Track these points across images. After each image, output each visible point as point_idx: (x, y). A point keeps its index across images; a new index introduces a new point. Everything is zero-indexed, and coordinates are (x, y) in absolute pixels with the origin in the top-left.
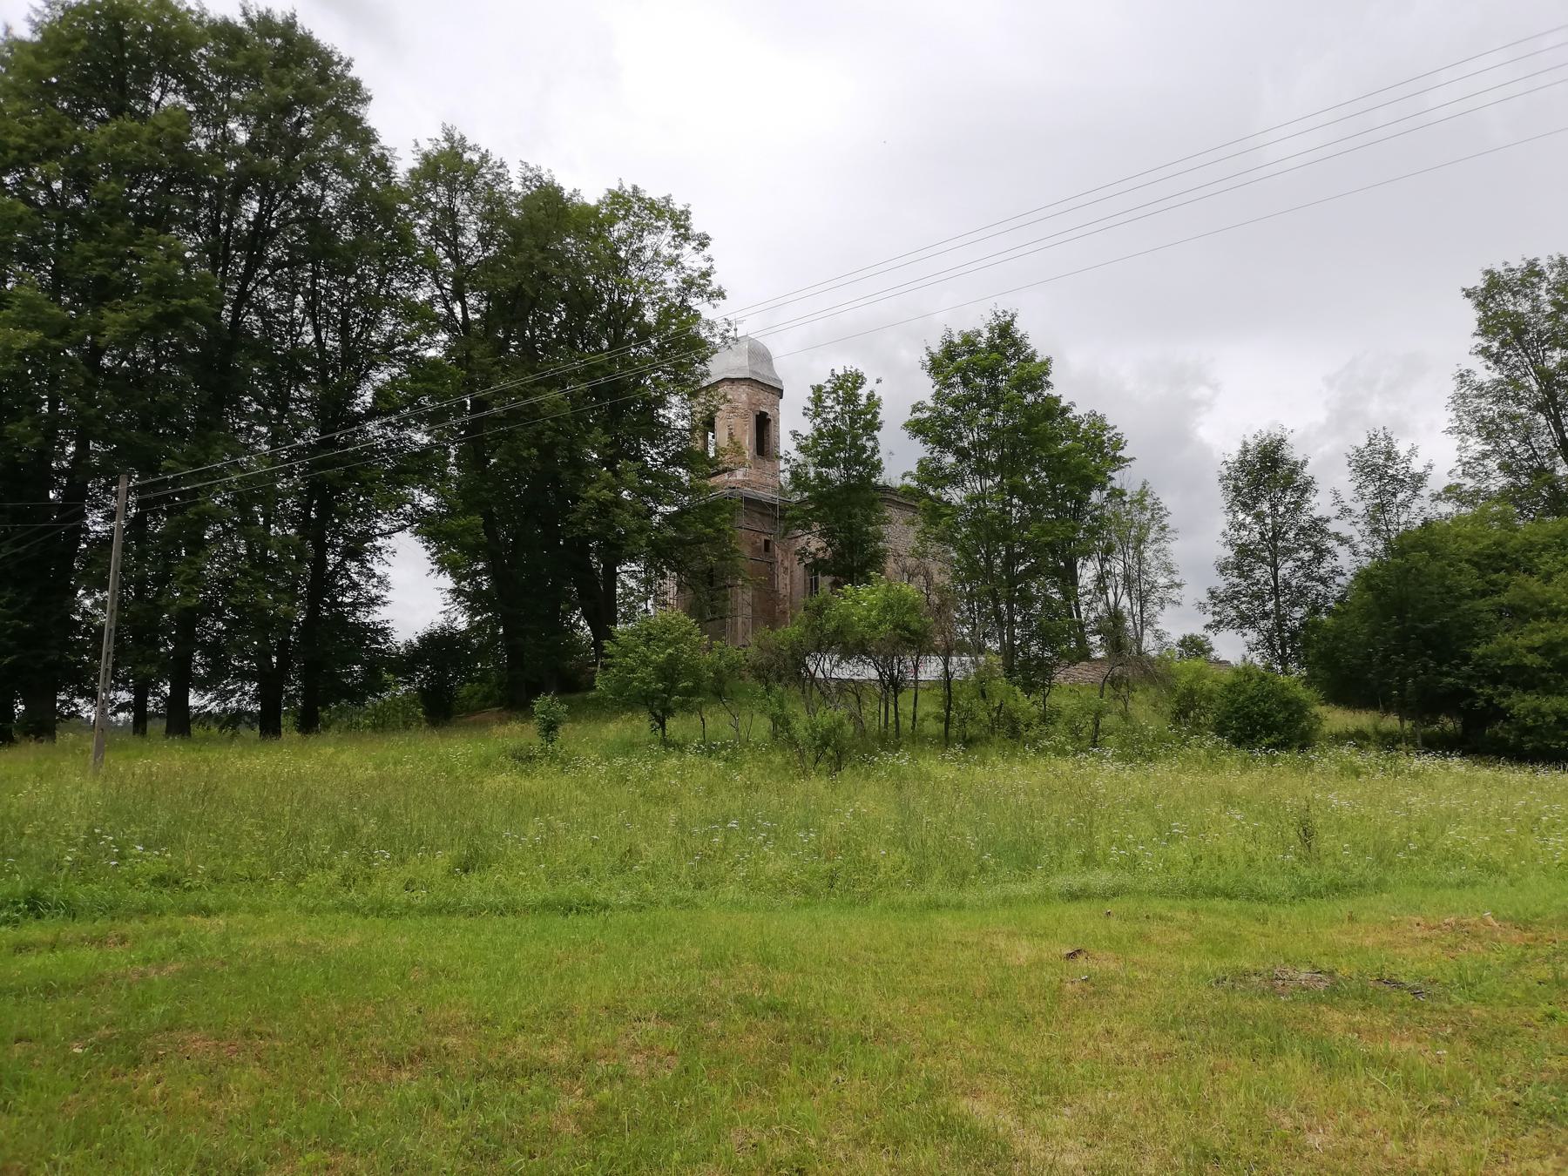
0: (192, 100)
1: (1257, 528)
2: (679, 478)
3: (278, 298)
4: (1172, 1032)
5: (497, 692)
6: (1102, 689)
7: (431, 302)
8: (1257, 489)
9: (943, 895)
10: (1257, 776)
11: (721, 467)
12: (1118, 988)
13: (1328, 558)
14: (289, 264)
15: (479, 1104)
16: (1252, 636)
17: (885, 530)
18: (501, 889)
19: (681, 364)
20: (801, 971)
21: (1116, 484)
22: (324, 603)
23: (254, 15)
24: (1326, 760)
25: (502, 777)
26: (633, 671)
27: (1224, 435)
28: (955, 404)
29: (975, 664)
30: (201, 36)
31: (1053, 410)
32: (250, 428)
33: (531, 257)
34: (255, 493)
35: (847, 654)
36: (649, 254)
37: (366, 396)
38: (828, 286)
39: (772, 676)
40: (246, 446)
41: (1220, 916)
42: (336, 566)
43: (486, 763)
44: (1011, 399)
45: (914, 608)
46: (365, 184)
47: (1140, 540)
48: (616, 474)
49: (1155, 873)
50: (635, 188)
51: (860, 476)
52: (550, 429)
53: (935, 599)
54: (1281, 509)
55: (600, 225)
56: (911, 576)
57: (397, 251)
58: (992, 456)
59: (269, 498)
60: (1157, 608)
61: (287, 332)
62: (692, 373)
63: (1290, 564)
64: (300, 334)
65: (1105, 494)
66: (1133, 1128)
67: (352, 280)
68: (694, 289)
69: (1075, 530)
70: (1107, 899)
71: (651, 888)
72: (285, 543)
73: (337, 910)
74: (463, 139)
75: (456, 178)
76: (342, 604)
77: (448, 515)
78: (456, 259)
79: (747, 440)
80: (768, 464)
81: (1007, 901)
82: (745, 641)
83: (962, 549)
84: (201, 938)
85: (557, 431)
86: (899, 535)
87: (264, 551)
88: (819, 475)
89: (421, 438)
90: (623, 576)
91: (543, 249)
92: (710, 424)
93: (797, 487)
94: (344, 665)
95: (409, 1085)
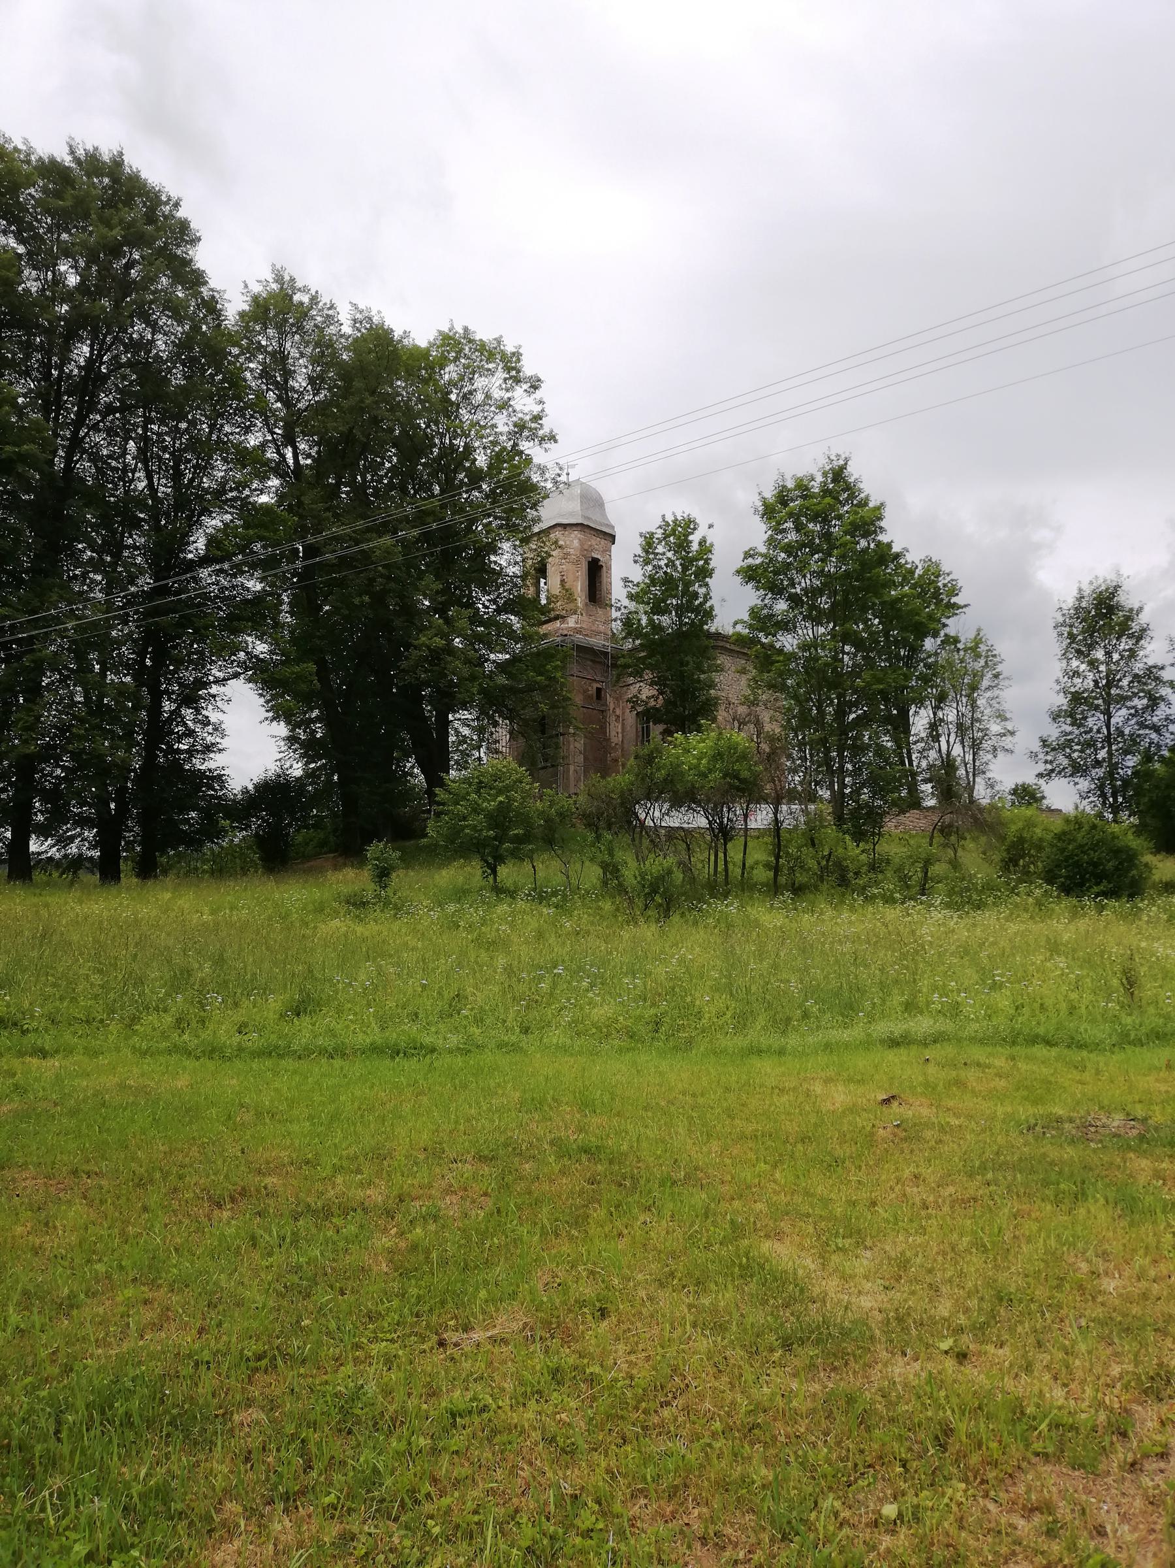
0: (21, 241)
1: (1090, 676)
2: (511, 625)
3: (109, 444)
4: (979, 1177)
5: (332, 839)
6: (932, 838)
7: (263, 446)
8: (1091, 636)
9: (764, 1042)
10: (1083, 924)
11: (552, 615)
12: (928, 1134)
13: (1162, 705)
14: (121, 410)
15: (295, 1242)
16: (1084, 784)
17: (717, 678)
18: (331, 1032)
19: (512, 510)
20: (618, 1114)
21: (951, 630)
22: (161, 750)
23: (80, 153)
24: (1152, 909)
25: (336, 923)
26: (465, 818)
27: (1063, 581)
28: (789, 549)
29: (805, 812)
30: (28, 176)
31: (885, 555)
32: (85, 575)
33: (362, 401)
34: (93, 639)
35: (677, 802)
36: (479, 397)
37: (199, 544)
38: (728, 434)
39: (602, 824)
40: (81, 593)
41: (1038, 1064)
42: (172, 712)
43: (320, 909)
44: (844, 545)
45: (744, 757)
46: (196, 328)
47: (974, 688)
48: (448, 621)
49: (977, 1020)
50: (466, 329)
51: (693, 623)
52: (382, 576)
53: (765, 747)
54: (1116, 657)
55: (430, 367)
56: (742, 723)
57: (229, 395)
58: (824, 602)
59: (105, 645)
60: (990, 756)
61: (120, 479)
62: (524, 518)
63: (1124, 712)
64: (133, 480)
65: (939, 641)
66: (930, 1271)
67: (183, 425)
68: (526, 433)
69: (907, 678)
70: (926, 1045)
71: (477, 1031)
72: (121, 691)
73: (170, 1052)
74: (292, 280)
75: (286, 320)
76: (179, 751)
77: (282, 663)
78: (288, 403)
79: (579, 587)
80: (600, 611)
81: (828, 1047)
82: (577, 789)
83: (796, 697)
84: (36, 1079)
85: (389, 578)
86: (731, 682)
87: (100, 698)
88: (651, 621)
89: (255, 586)
90: (456, 724)
91: (373, 393)
92: (542, 571)
93: (629, 634)
94: (181, 812)
95: (229, 1223)
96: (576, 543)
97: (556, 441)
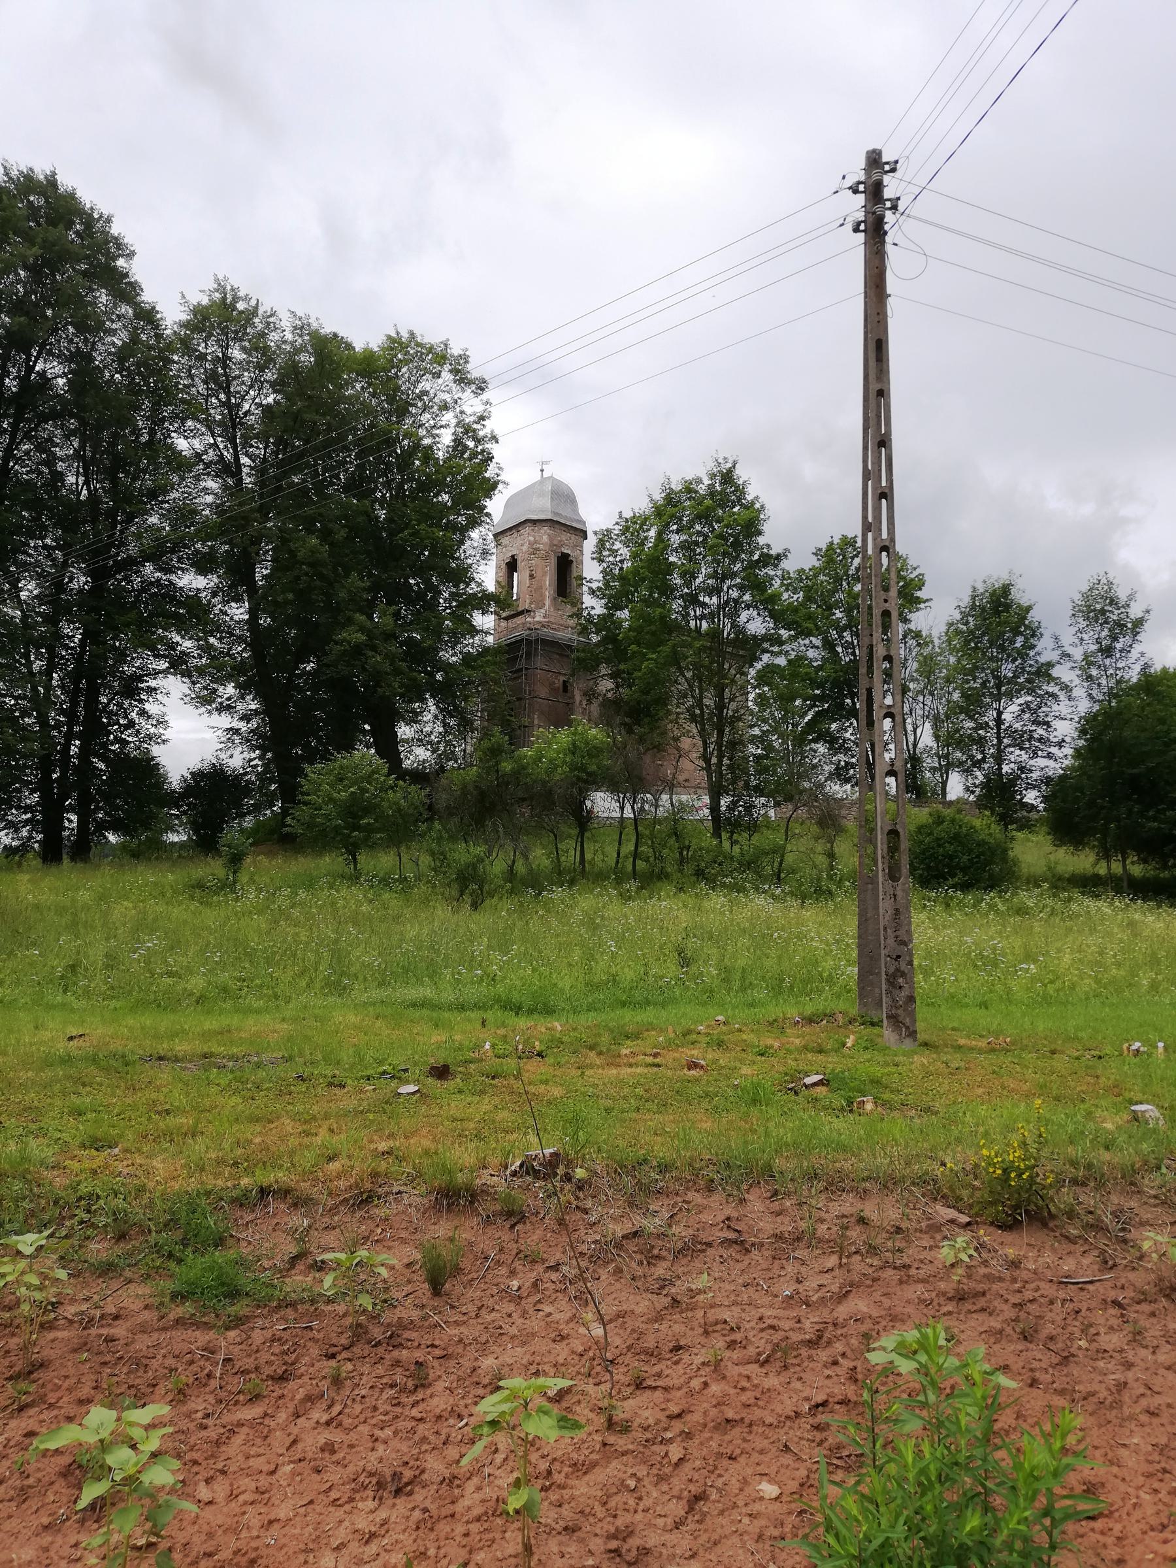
79: (548, 581)
96: (545, 538)
97: (497, 442)
